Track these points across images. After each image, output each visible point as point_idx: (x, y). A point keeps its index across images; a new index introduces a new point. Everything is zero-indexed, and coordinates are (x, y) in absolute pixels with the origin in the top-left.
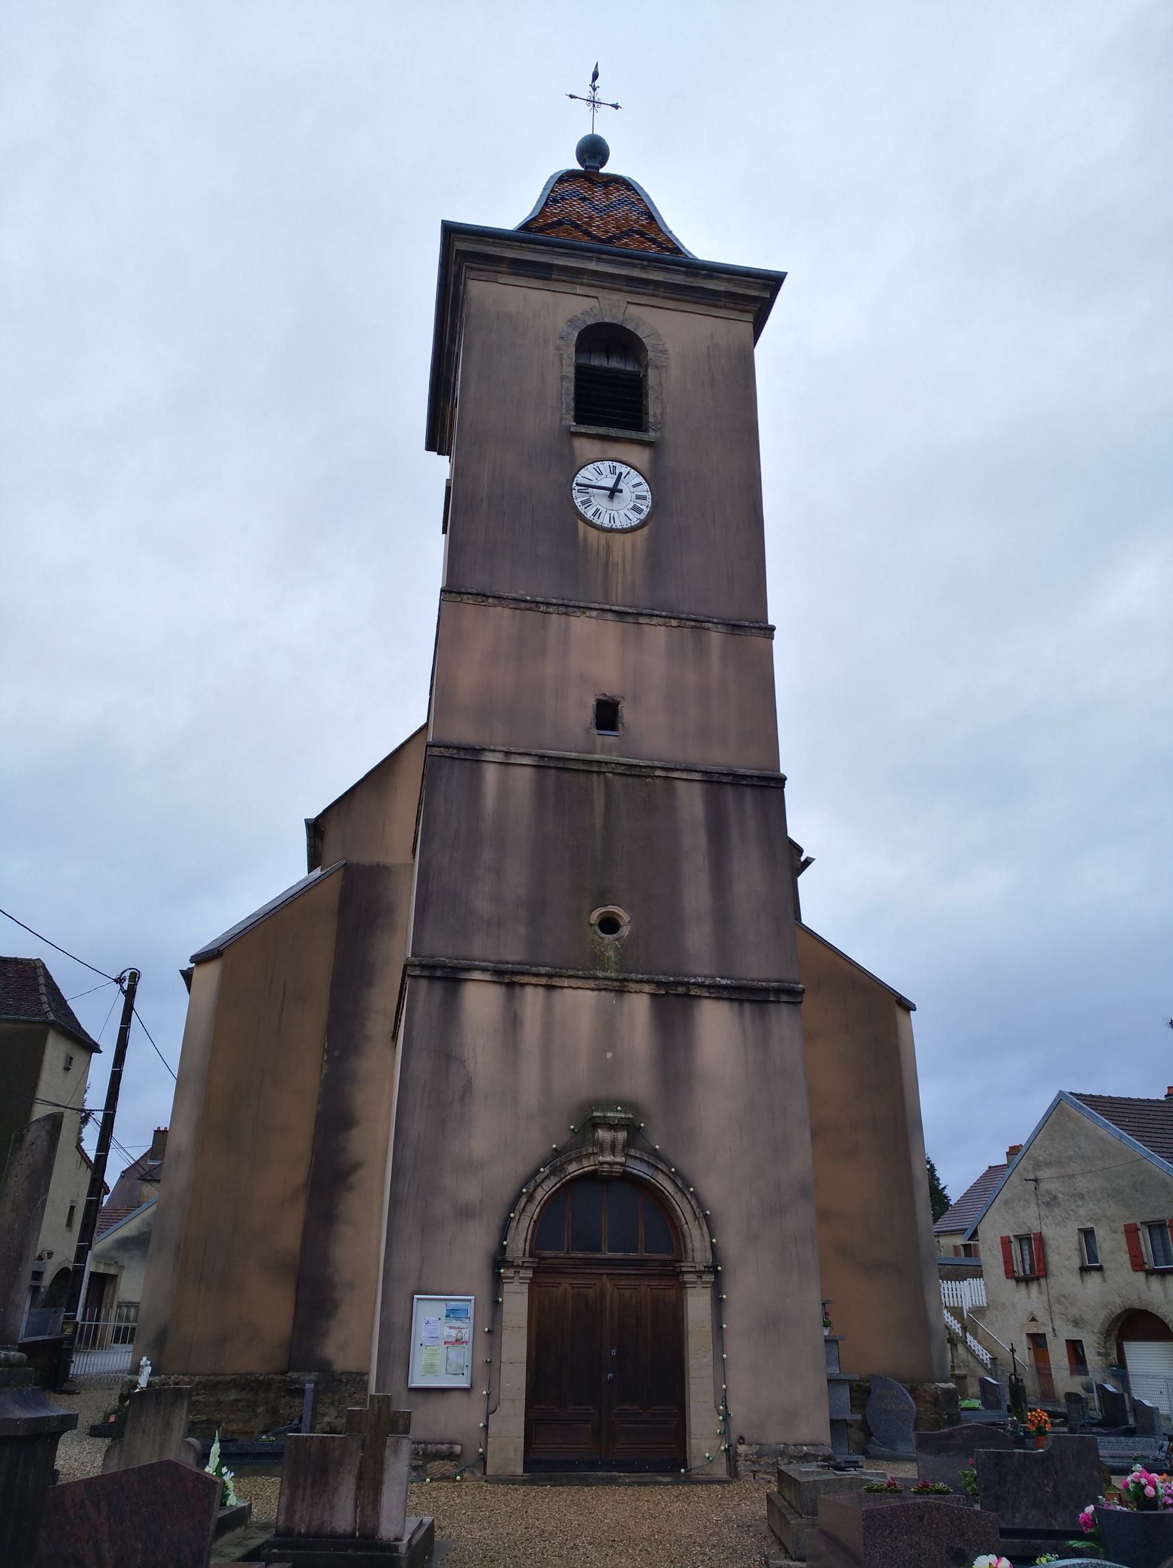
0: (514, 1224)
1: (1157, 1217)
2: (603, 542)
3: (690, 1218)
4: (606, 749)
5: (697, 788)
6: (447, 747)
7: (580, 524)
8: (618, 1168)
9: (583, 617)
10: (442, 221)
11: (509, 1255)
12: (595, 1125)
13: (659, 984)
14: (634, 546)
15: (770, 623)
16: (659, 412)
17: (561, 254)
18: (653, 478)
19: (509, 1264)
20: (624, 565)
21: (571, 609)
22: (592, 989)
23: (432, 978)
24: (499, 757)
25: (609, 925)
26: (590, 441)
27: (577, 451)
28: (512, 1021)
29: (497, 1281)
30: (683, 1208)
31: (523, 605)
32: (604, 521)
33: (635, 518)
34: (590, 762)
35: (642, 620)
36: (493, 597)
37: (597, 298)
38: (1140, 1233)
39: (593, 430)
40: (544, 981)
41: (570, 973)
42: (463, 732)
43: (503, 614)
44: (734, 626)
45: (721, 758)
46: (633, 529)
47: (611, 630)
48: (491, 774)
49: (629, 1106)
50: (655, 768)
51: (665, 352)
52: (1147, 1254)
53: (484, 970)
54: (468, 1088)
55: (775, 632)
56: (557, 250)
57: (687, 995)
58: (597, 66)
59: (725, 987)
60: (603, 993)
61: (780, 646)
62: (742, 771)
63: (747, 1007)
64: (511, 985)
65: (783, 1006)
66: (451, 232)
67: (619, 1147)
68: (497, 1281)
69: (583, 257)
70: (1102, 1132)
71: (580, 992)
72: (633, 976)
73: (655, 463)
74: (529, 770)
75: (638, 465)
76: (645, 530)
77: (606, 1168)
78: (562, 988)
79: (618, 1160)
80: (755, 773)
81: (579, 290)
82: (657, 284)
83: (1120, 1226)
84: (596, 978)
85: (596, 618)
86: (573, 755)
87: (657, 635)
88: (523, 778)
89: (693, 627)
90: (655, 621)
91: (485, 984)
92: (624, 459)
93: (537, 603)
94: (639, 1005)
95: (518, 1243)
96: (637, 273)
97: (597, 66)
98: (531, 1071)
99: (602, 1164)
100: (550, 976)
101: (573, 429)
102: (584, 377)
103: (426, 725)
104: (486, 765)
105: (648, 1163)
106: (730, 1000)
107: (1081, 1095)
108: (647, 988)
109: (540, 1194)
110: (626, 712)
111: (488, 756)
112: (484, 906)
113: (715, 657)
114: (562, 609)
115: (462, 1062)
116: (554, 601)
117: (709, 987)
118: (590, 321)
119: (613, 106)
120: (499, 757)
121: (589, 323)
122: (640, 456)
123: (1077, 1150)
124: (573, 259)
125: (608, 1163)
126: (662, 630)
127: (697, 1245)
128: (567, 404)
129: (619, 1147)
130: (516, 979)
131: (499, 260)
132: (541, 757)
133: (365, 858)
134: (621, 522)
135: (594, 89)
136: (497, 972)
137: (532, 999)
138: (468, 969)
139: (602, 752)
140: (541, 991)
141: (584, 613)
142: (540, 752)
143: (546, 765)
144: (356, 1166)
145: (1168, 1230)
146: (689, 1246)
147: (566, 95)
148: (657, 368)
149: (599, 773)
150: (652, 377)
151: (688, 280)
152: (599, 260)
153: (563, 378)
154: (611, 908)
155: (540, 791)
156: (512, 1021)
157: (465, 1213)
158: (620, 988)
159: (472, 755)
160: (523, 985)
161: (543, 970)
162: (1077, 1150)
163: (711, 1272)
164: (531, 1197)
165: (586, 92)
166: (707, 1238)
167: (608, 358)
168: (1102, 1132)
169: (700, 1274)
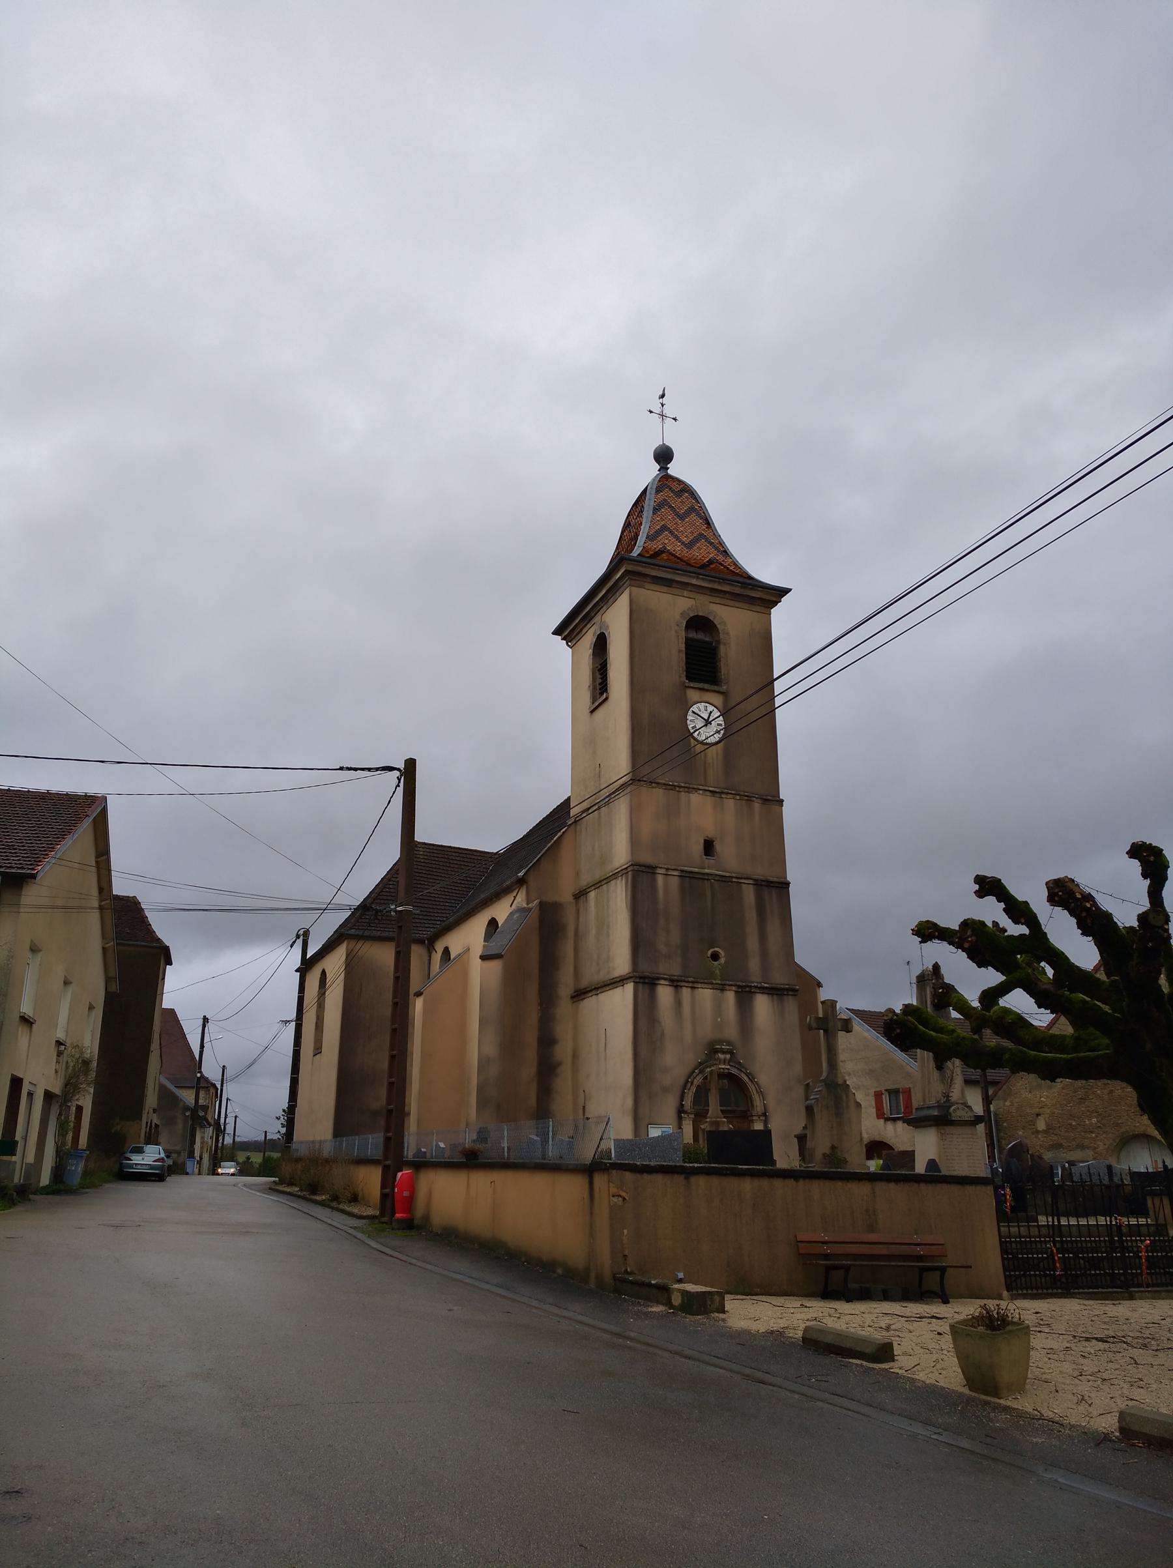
0: (686, 1095)
1: (896, 1086)
3: (755, 1092)
6: (640, 866)
7: (692, 740)
8: (726, 1071)
9: (696, 794)
10: (936, 962)
11: (685, 1109)
12: (716, 1051)
13: (739, 986)
15: (781, 798)
17: (678, 574)
20: (713, 763)
21: (691, 789)
22: (711, 989)
23: (644, 983)
26: (694, 690)
27: (688, 697)
28: (678, 1003)
29: (680, 1119)
30: (752, 1088)
31: (669, 787)
33: (717, 737)
34: (703, 874)
35: (723, 796)
36: (655, 783)
37: (694, 599)
38: (884, 1096)
39: (697, 685)
40: (690, 985)
41: (702, 981)
42: (647, 858)
43: (659, 792)
44: (766, 800)
45: (762, 871)
47: (709, 801)
48: (660, 879)
49: (729, 1043)
50: (732, 877)
51: (728, 634)
52: (887, 1109)
53: (665, 979)
54: (663, 1034)
55: (784, 803)
56: (677, 572)
57: (751, 992)
58: (664, 390)
59: (766, 988)
60: (715, 990)
61: (786, 809)
62: (771, 879)
63: (775, 996)
64: (676, 987)
65: (790, 997)
67: (727, 1062)
68: (680, 1119)
70: (866, 1034)
71: (706, 990)
72: (727, 982)
73: (725, 703)
74: (676, 877)
75: (717, 705)
76: (720, 745)
77: (722, 1070)
78: (698, 988)
79: (727, 1067)
80: (775, 880)
81: (686, 593)
82: (725, 592)
83: (872, 1092)
84: (713, 984)
85: (702, 794)
86: (696, 870)
87: (730, 803)
88: (674, 882)
89: (747, 800)
91: (665, 986)
92: (711, 701)
93: (675, 786)
94: (730, 996)
95: (688, 1102)
96: (716, 586)
97: (664, 390)
98: (687, 1025)
99: (720, 1069)
100: (693, 982)
101: (687, 685)
102: (690, 644)
104: (658, 875)
105: (737, 1068)
106: (768, 994)
107: (853, 1010)
108: (734, 988)
110: (718, 846)
112: (663, 949)
114: (686, 790)
115: (659, 1022)
116: (683, 785)
117: (759, 988)
119: (673, 419)
121: (691, 616)
122: (718, 700)
123: (848, 1045)
124: (684, 577)
125: (723, 1069)
126: (731, 802)
127: (758, 1104)
128: (683, 668)
129: (727, 1062)
130: (679, 984)
131: (646, 576)
132: (682, 871)
133: (549, 898)
134: (712, 740)
135: (663, 405)
136: (672, 981)
137: (686, 992)
138: (659, 979)
140: (689, 989)
141: (696, 791)
143: (685, 876)
144: (559, 1064)
145: (901, 1094)
146: (755, 1105)
147: (664, 456)
148: (725, 644)
149: (708, 879)
150: (722, 650)
151: (742, 590)
152: (698, 578)
153: (680, 651)
154: (717, 949)
155: (682, 889)
156: (678, 1003)
157: (665, 1090)
158: (722, 988)
160: (681, 986)
161: (691, 979)
162: (848, 1045)
163: (763, 1116)
165: (657, 409)
166: (762, 1101)
167: (696, 632)
168: (866, 1034)
169: (759, 1116)
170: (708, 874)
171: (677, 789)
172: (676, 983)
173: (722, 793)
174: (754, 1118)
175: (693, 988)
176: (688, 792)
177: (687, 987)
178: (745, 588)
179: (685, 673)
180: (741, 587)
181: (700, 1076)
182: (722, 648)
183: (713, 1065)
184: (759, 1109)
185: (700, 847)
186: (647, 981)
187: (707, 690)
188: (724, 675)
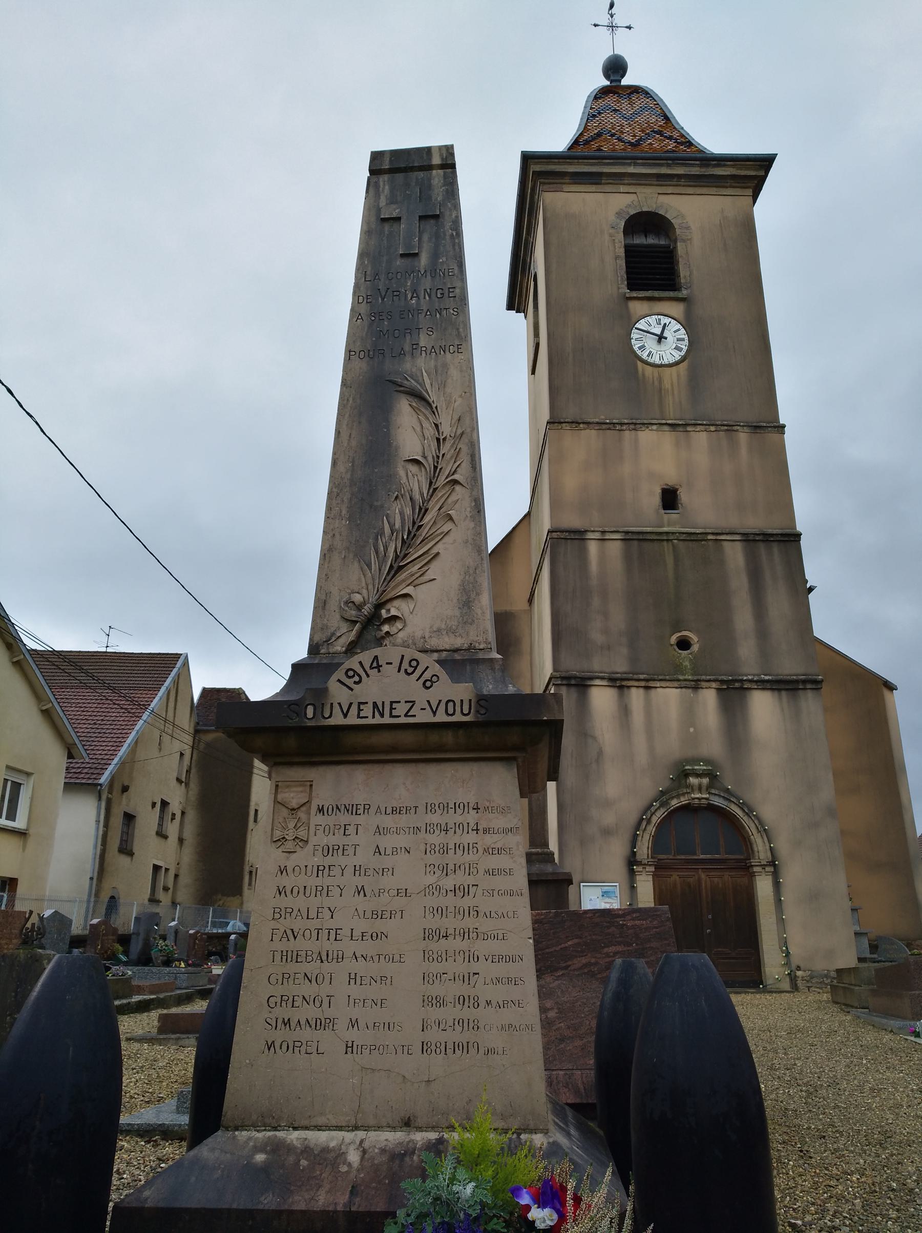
2: (656, 375)
3: (754, 831)
4: (671, 522)
5: (739, 546)
7: (639, 363)
8: (704, 801)
11: (639, 858)
14: (678, 376)
16: (688, 274)
18: (688, 324)
19: (639, 863)
21: (638, 426)
24: (597, 535)
25: (684, 644)
28: (625, 711)
29: (632, 873)
31: (604, 426)
32: (656, 360)
33: (678, 356)
35: (689, 429)
36: (583, 423)
40: (643, 684)
41: (660, 677)
42: (572, 521)
46: (677, 363)
48: (593, 548)
51: (688, 228)
53: (602, 678)
54: (600, 753)
62: (770, 531)
64: (621, 687)
66: (527, 158)
68: (632, 873)
69: (624, 164)
75: (676, 316)
76: (685, 364)
78: (656, 687)
80: (779, 531)
81: (622, 188)
82: (679, 177)
86: (649, 529)
87: (701, 438)
88: (615, 548)
90: (699, 428)
94: (709, 697)
96: (664, 170)
100: (647, 680)
101: (627, 295)
103: (528, 515)
108: (714, 685)
109: (655, 819)
111: (590, 535)
112: (597, 637)
113: (744, 451)
114: (632, 427)
116: (626, 421)
118: (632, 212)
119: (627, 27)
120: (597, 535)
122: (677, 309)
126: (704, 435)
127: (761, 848)
128: (622, 276)
129: (704, 788)
130: (624, 683)
132: (627, 533)
134: (668, 359)
135: (612, 16)
139: (669, 525)
142: (626, 529)
148: (684, 241)
152: (636, 164)
153: (617, 258)
155: (627, 557)
156: (625, 711)
157: (607, 832)
158: (696, 686)
159: (578, 536)
161: (642, 677)
164: (649, 821)
165: (605, 19)
167: (646, 237)
169: (763, 866)
170: (667, 533)
171: (618, 427)
172: (619, 683)
173: (687, 425)
174: (755, 869)
175: (647, 688)
176: (634, 429)
177: (637, 687)
178: (707, 166)
179: (626, 283)
180: (701, 166)
181: (662, 810)
182: (680, 246)
183: (683, 794)
184: (762, 856)
185: (656, 499)
186: (573, 682)
187: (660, 299)
188: (685, 277)
